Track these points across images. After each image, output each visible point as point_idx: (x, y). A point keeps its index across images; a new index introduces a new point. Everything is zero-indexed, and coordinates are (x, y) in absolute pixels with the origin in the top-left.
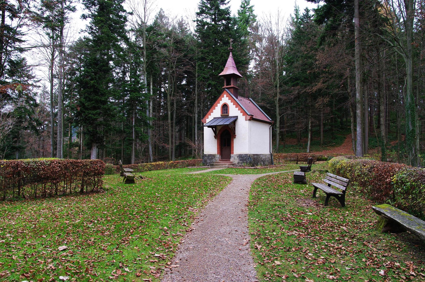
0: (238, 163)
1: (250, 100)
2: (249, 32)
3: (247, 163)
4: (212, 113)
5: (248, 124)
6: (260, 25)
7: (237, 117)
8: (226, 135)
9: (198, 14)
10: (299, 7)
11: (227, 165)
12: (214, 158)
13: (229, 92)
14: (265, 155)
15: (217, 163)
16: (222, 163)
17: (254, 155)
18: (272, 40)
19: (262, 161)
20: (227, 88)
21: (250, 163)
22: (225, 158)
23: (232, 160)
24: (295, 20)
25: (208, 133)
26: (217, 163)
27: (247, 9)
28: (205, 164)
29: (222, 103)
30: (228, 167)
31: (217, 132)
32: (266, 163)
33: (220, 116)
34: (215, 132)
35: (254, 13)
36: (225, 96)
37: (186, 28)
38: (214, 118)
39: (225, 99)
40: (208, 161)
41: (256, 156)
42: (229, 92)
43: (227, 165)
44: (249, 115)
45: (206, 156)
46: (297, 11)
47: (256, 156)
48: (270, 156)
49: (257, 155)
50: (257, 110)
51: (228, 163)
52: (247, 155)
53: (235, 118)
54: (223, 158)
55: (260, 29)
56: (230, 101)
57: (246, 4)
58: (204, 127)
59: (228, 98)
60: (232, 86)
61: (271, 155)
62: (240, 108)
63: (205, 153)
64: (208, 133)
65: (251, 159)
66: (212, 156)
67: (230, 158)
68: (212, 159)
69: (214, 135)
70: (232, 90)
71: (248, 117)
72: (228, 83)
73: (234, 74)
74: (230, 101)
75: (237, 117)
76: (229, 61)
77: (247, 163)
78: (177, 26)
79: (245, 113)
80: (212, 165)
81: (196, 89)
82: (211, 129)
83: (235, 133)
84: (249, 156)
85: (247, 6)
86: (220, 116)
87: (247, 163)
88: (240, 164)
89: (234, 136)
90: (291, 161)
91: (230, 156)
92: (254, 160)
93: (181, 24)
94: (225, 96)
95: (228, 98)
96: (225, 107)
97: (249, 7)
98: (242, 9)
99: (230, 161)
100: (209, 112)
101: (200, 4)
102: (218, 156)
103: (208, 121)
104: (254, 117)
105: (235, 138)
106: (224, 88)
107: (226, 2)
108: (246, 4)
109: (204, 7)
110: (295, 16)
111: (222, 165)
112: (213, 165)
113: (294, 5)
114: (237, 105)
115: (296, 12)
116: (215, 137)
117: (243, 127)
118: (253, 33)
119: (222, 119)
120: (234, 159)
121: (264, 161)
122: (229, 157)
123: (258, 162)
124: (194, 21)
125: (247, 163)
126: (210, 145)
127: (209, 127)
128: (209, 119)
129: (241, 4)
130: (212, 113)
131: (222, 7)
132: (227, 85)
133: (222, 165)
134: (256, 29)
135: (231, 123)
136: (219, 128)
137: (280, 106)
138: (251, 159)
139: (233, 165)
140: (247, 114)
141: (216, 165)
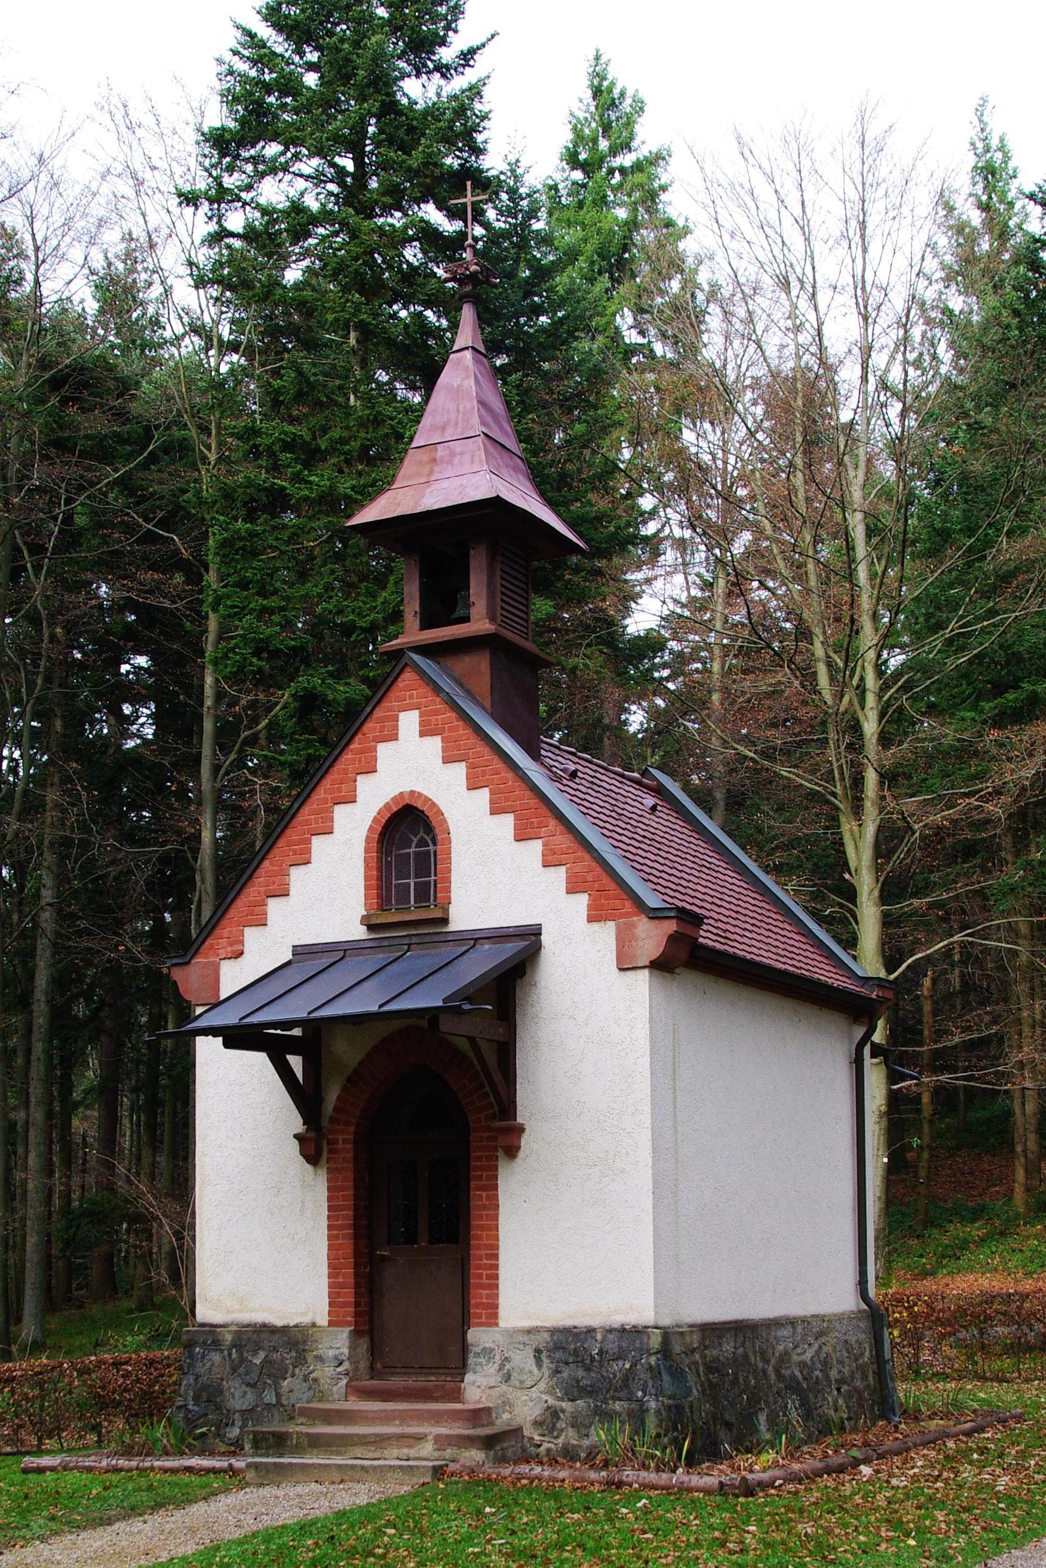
0: (550, 1421)
1: (659, 791)
2: (631, 351)
3: (638, 1417)
4: (274, 906)
5: (642, 1011)
6: (713, 294)
7: (529, 939)
8: (420, 1111)
9: (221, 143)
10: (1011, 144)
11: (427, 1449)
12: (301, 1360)
13: (446, 684)
14: (815, 1327)
15: (329, 1416)
16: (379, 1417)
17: (712, 1331)
18: (802, 406)
19: (793, 1386)
20: (429, 650)
21: (675, 1418)
22: (407, 1369)
23: (479, 1386)
24: (985, 245)
25: (238, 1103)
26: (329, 1416)
27: (617, 178)
28: (203, 1424)
29: (374, 794)
30: (438, 1472)
31: (332, 1096)
32: (833, 1405)
33: (360, 933)
34: (304, 1096)
35: (675, 204)
36: (409, 721)
37: (156, 323)
38: (302, 952)
39: (409, 759)
40: (238, 1397)
41: (728, 1347)
42: (446, 684)
43: (427, 1449)
44: (655, 915)
45: (216, 1344)
46: (991, 173)
47: (728, 1347)
48: (860, 1336)
49: (740, 1329)
50: (731, 878)
51: (436, 1417)
52: (638, 1332)
53: (511, 948)
54: (391, 1369)
55: (714, 320)
56: (459, 771)
57: (604, 144)
58: (200, 1041)
59: (435, 744)
60: (479, 624)
61: (875, 1317)
62: (564, 841)
63: (205, 1313)
64: (238, 1103)
65: (677, 1374)
66: (273, 1348)
67: (462, 1368)
68: (274, 1372)
69: (297, 1124)
70: (480, 665)
71: (651, 939)
72: (443, 605)
73: (497, 503)
74: (459, 771)
75: (529, 939)
76: (456, 392)
77: (639, 1429)
78: (92, 306)
79: (608, 896)
80: (277, 1446)
81: (207, 750)
82: (260, 1060)
83: (507, 1106)
84: (665, 1350)
85: (614, 151)
86: (360, 933)
87: (638, 1417)
88: (569, 1436)
89: (506, 1136)
90: (1017, 1349)
91: (464, 1348)
92: (711, 1391)
93: (117, 294)
94: (409, 721)
95: (435, 744)
96: (408, 838)
97: (626, 160)
98: (578, 175)
99: (456, 1395)
100: (251, 893)
101: (242, 66)
102: (338, 1343)
103: (233, 977)
104: (706, 938)
105: (512, 1151)
106: (397, 655)
107: (446, 54)
108: (604, 144)
109: (268, 88)
110: (976, 218)
111: (380, 1441)
112: (279, 1442)
113: (972, 132)
114: (534, 816)
115: (989, 188)
116: (312, 1147)
117: (598, 1026)
118: (659, 349)
119: (381, 957)
120: (502, 1381)
121: (806, 1391)
122: (454, 1360)
123: (754, 1401)
124: (189, 199)
125: (639, 1429)
126: (259, 1229)
127: (237, 1038)
128: (252, 957)
129: (566, 137)
130: (274, 906)
131: (417, 91)
132: (427, 623)
133: (380, 1441)
134: (684, 320)
135: (472, 993)
136: (347, 1052)
137: (888, 894)
138: (677, 1374)
139: (489, 1443)
140: (640, 905)
141: (316, 1443)
